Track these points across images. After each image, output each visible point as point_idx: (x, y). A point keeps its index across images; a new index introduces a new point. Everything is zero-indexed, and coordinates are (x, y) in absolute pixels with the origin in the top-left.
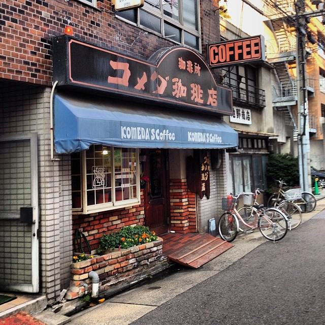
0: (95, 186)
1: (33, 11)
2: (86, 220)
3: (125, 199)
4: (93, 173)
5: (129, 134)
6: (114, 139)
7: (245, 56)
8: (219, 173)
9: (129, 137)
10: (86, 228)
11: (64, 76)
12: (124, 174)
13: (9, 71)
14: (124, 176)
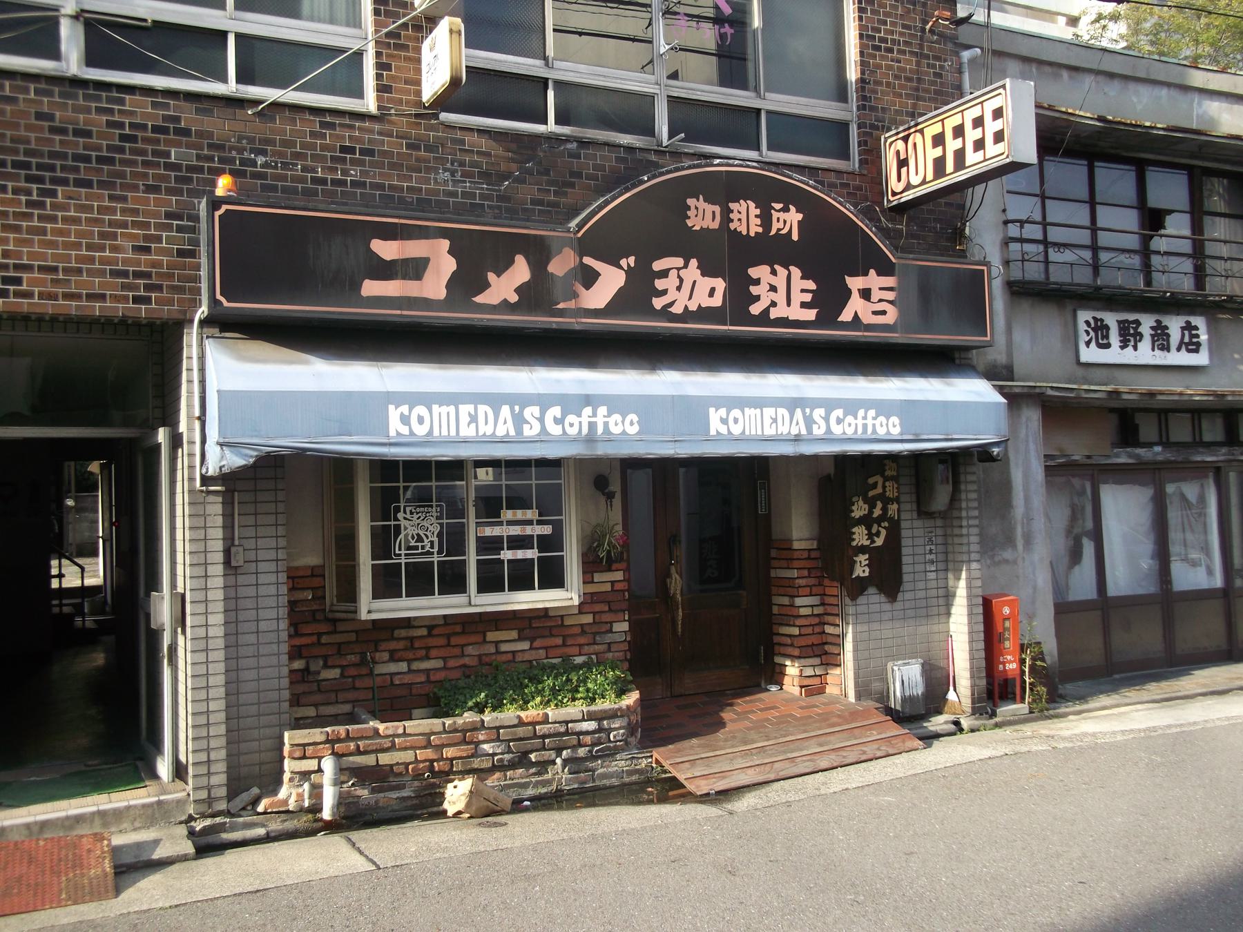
1: (143, 152)
3: (544, 586)
4: (396, 519)
7: (971, 157)
8: (953, 526)
10: (399, 654)
11: (1206, 242)
13: (67, 296)
14: (515, 531)
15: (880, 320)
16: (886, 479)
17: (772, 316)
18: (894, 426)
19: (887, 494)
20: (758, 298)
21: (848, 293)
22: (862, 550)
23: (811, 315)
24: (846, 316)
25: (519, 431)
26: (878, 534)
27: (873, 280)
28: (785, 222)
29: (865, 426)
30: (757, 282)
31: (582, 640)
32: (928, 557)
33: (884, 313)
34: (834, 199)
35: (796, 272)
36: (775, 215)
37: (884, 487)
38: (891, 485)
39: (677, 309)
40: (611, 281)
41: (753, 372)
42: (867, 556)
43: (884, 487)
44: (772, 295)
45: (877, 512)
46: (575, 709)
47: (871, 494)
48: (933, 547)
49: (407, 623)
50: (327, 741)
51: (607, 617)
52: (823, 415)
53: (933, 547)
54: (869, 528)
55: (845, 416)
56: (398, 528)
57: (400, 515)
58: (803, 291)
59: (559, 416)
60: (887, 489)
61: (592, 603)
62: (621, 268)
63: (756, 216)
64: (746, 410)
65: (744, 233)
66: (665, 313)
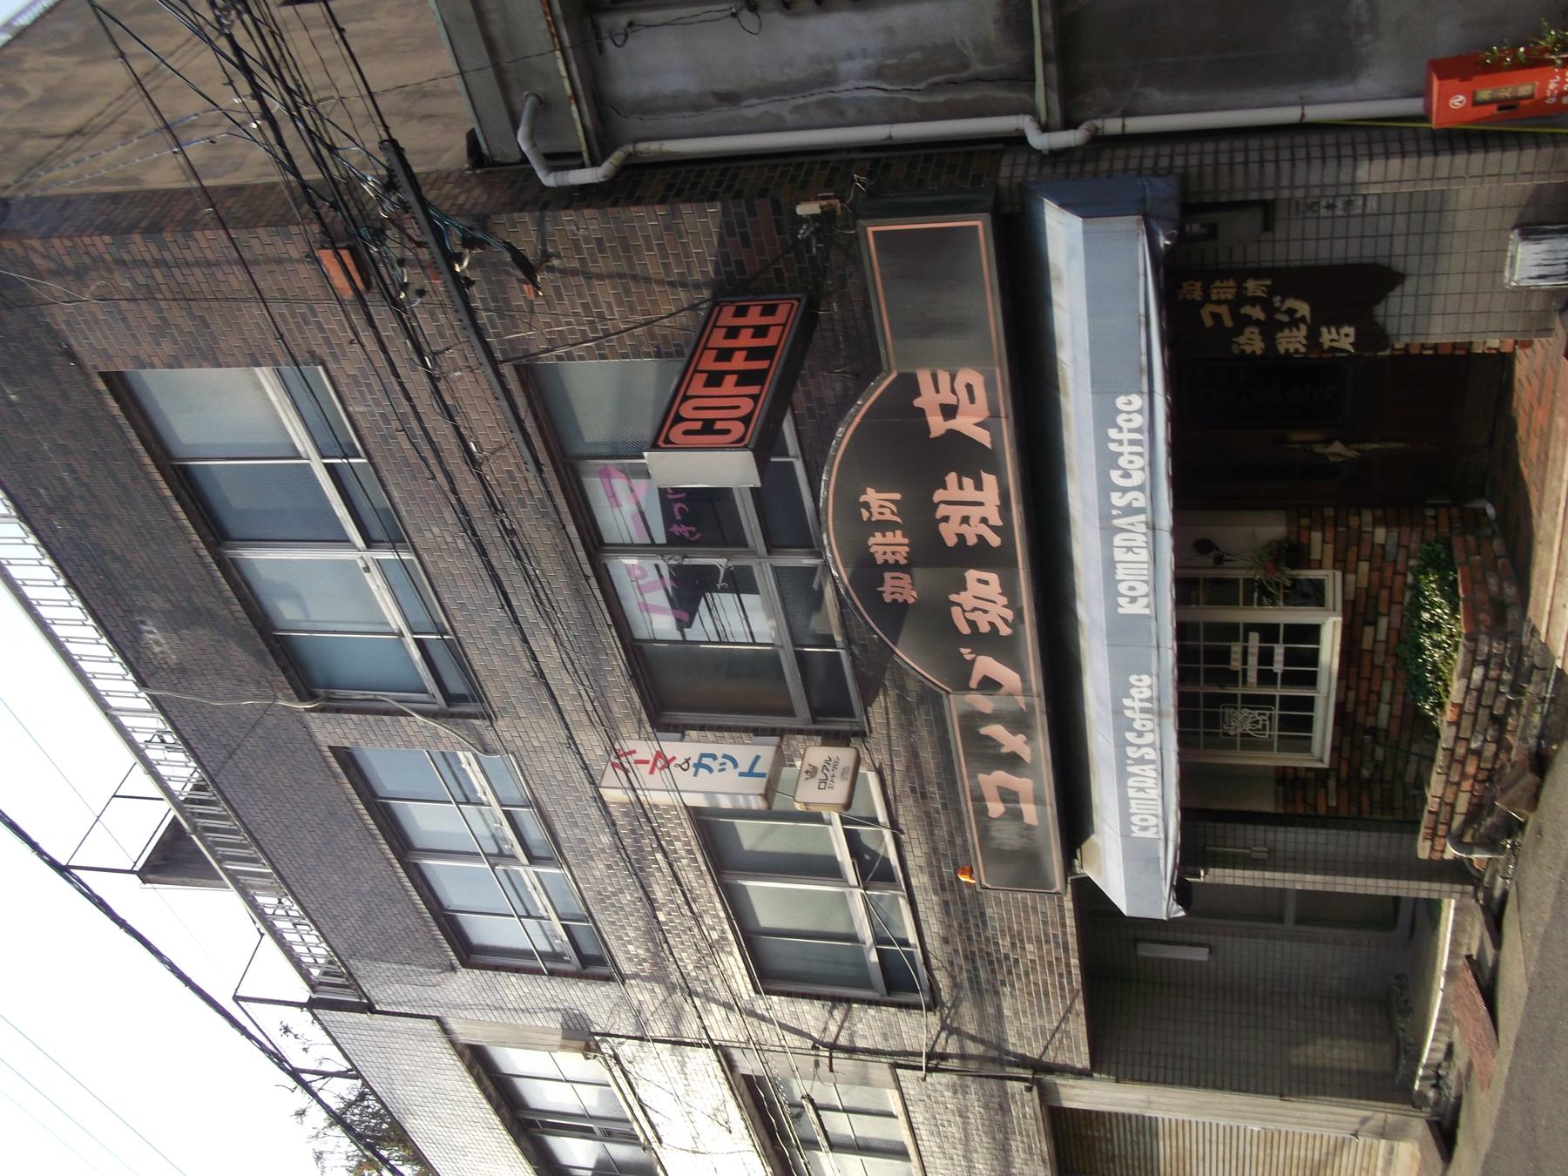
0: (1267, 733)
2: (1350, 708)
3: (1317, 640)
5: (1146, 820)
6: (1162, 862)
9: (1153, 821)
12: (1245, 661)
14: (1253, 661)
15: (980, 393)
16: (1207, 299)
17: (999, 523)
18: (1130, 403)
19: (1230, 297)
20: (980, 537)
21: (952, 434)
22: (1313, 336)
23: (989, 480)
24: (983, 437)
25: (1140, 511)
26: (1291, 312)
27: (928, 400)
28: (881, 506)
29: (1132, 442)
30: (961, 537)
31: (1389, 572)
32: (1339, 212)
33: (969, 388)
34: (836, 450)
35: (939, 495)
36: (876, 517)
37: (1219, 302)
38: (1215, 291)
39: (1009, 614)
40: (987, 665)
41: (1057, 374)
42: (1324, 330)
43: (1219, 302)
44: (974, 521)
45: (1257, 313)
46: (1457, 687)
47: (1228, 322)
48: (1324, 202)
49: (1340, 707)
50: (1432, 840)
51: (1366, 550)
52: (1120, 494)
53: (1324, 202)
54: (1281, 326)
55: (1120, 468)
56: (1243, 735)
57: (1232, 733)
58: (961, 487)
59: (1120, 472)
60: (1223, 297)
61: (1345, 561)
62: (973, 661)
63: (884, 536)
64: (1118, 577)
65: (907, 549)
66: (1004, 531)
